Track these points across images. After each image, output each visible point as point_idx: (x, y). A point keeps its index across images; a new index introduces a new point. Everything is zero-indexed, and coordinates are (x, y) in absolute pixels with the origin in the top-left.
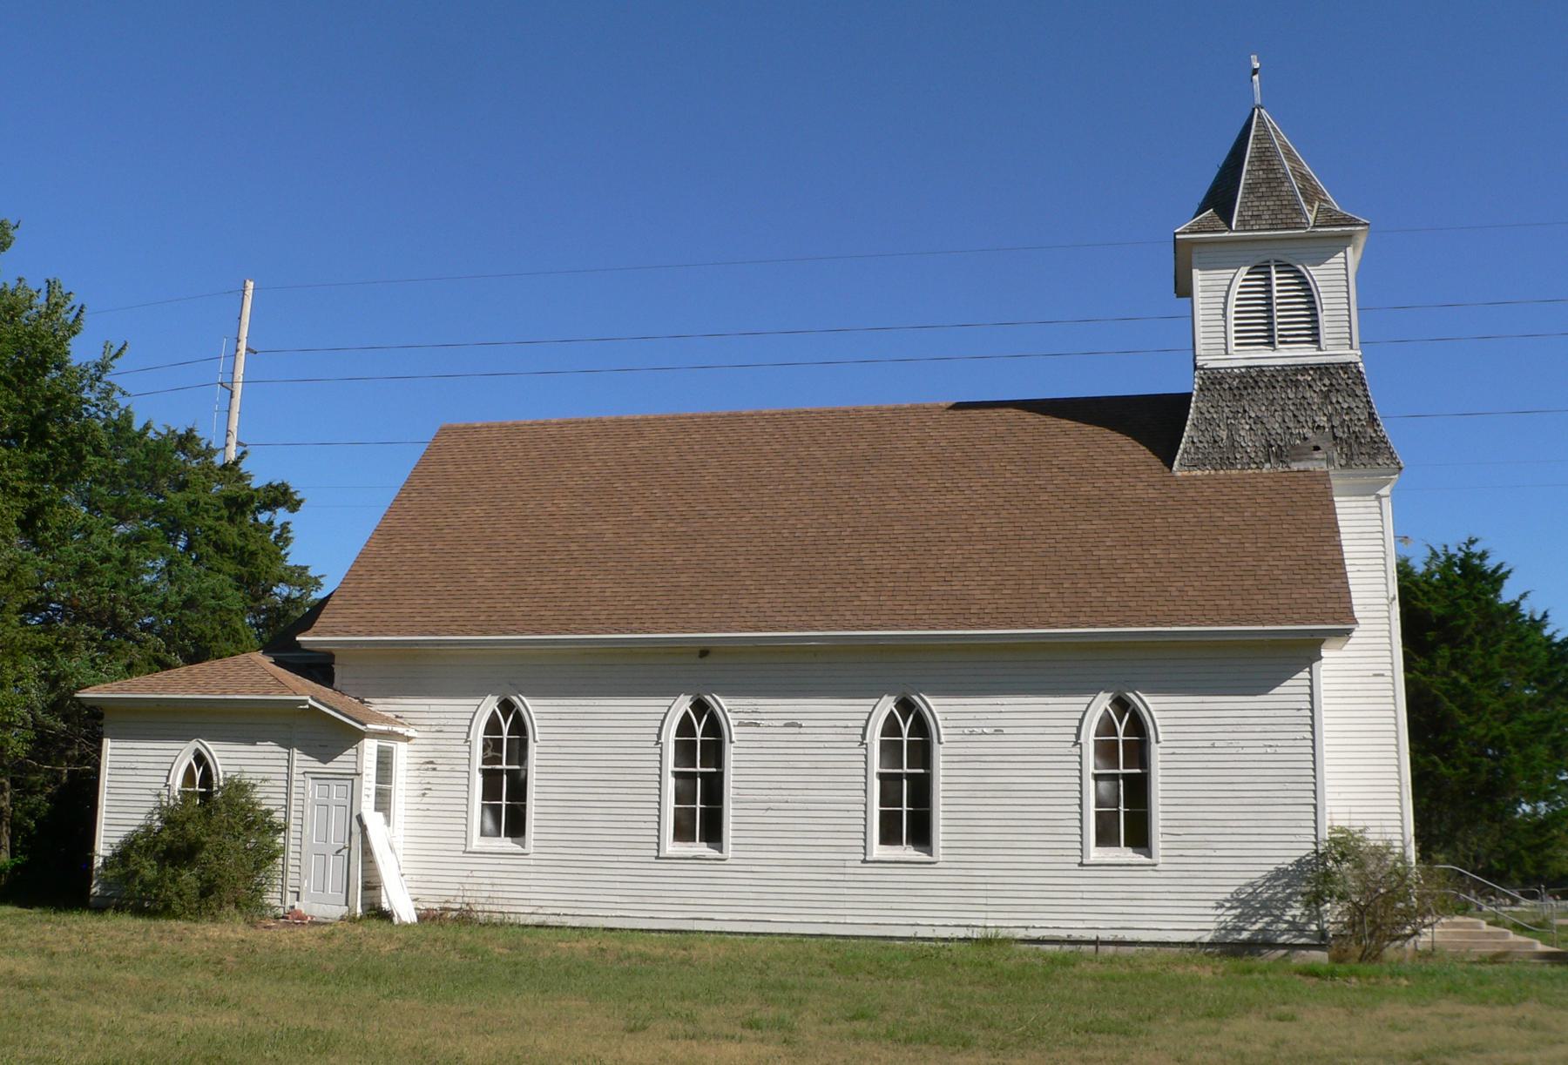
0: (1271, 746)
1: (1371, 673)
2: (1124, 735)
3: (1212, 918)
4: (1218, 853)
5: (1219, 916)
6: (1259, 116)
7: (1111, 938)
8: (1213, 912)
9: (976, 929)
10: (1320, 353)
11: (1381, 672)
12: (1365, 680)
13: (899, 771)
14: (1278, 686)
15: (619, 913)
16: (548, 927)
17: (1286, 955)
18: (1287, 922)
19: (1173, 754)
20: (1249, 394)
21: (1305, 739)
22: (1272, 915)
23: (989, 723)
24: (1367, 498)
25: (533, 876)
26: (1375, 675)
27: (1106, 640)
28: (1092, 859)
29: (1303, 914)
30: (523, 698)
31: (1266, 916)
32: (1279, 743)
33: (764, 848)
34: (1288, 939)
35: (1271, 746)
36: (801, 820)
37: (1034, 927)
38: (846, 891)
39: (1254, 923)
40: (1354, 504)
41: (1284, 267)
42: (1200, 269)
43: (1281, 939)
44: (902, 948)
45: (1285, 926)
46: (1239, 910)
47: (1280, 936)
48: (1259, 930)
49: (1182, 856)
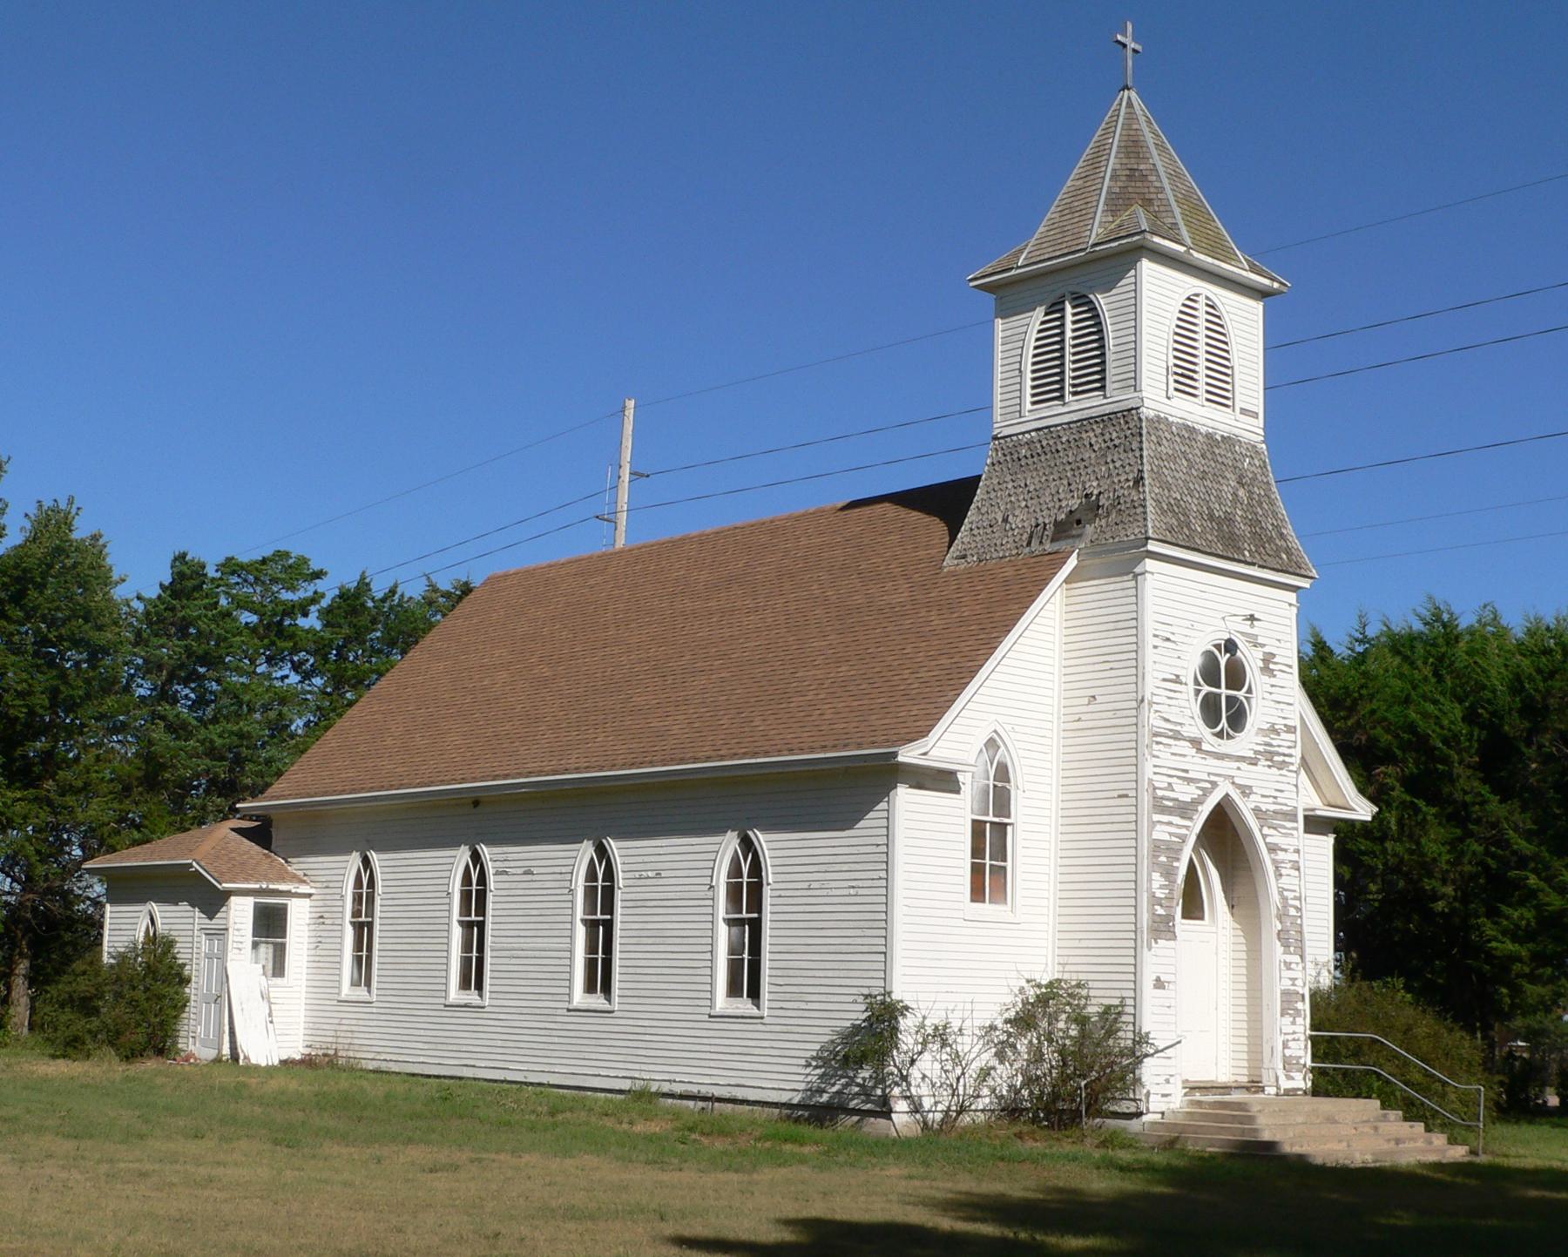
0: (853, 887)
1: (1115, 794)
2: (748, 877)
3: (801, 1078)
4: (810, 1006)
5: (808, 1075)
6: (1129, 98)
7: (728, 1096)
8: (803, 1071)
9: (637, 1081)
10: (1105, 401)
11: (1125, 792)
12: (1111, 802)
13: (594, 917)
14: (862, 819)
15: (422, 1059)
16: (382, 1072)
17: (858, 1121)
18: (858, 1085)
19: (780, 896)
20: (1034, 463)
21: (880, 878)
22: (847, 1077)
23: (648, 866)
24: (1125, 578)
25: (375, 1023)
26: (1120, 796)
27: (739, 773)
28: (575, 1004)
29: (871, 1077)
30: (758, 833)
31: (844, 1077)
32: (860, 883)
33: (508, 996)
34: (858, 1104)
35: (853, 887)
36: (531, 968)
37: (675, 1081)
38: (556, 1040)
39: (834, 1085)
40: (1112, 587)
41: (1081, 300)
42: (1002, 318)
43: (852, 1104)
44: (607, 1100)
45: (857, 1089)
46: (823, 1070)
47: (852, 1099)
48: (837, 1092)
49: (782, 1008)
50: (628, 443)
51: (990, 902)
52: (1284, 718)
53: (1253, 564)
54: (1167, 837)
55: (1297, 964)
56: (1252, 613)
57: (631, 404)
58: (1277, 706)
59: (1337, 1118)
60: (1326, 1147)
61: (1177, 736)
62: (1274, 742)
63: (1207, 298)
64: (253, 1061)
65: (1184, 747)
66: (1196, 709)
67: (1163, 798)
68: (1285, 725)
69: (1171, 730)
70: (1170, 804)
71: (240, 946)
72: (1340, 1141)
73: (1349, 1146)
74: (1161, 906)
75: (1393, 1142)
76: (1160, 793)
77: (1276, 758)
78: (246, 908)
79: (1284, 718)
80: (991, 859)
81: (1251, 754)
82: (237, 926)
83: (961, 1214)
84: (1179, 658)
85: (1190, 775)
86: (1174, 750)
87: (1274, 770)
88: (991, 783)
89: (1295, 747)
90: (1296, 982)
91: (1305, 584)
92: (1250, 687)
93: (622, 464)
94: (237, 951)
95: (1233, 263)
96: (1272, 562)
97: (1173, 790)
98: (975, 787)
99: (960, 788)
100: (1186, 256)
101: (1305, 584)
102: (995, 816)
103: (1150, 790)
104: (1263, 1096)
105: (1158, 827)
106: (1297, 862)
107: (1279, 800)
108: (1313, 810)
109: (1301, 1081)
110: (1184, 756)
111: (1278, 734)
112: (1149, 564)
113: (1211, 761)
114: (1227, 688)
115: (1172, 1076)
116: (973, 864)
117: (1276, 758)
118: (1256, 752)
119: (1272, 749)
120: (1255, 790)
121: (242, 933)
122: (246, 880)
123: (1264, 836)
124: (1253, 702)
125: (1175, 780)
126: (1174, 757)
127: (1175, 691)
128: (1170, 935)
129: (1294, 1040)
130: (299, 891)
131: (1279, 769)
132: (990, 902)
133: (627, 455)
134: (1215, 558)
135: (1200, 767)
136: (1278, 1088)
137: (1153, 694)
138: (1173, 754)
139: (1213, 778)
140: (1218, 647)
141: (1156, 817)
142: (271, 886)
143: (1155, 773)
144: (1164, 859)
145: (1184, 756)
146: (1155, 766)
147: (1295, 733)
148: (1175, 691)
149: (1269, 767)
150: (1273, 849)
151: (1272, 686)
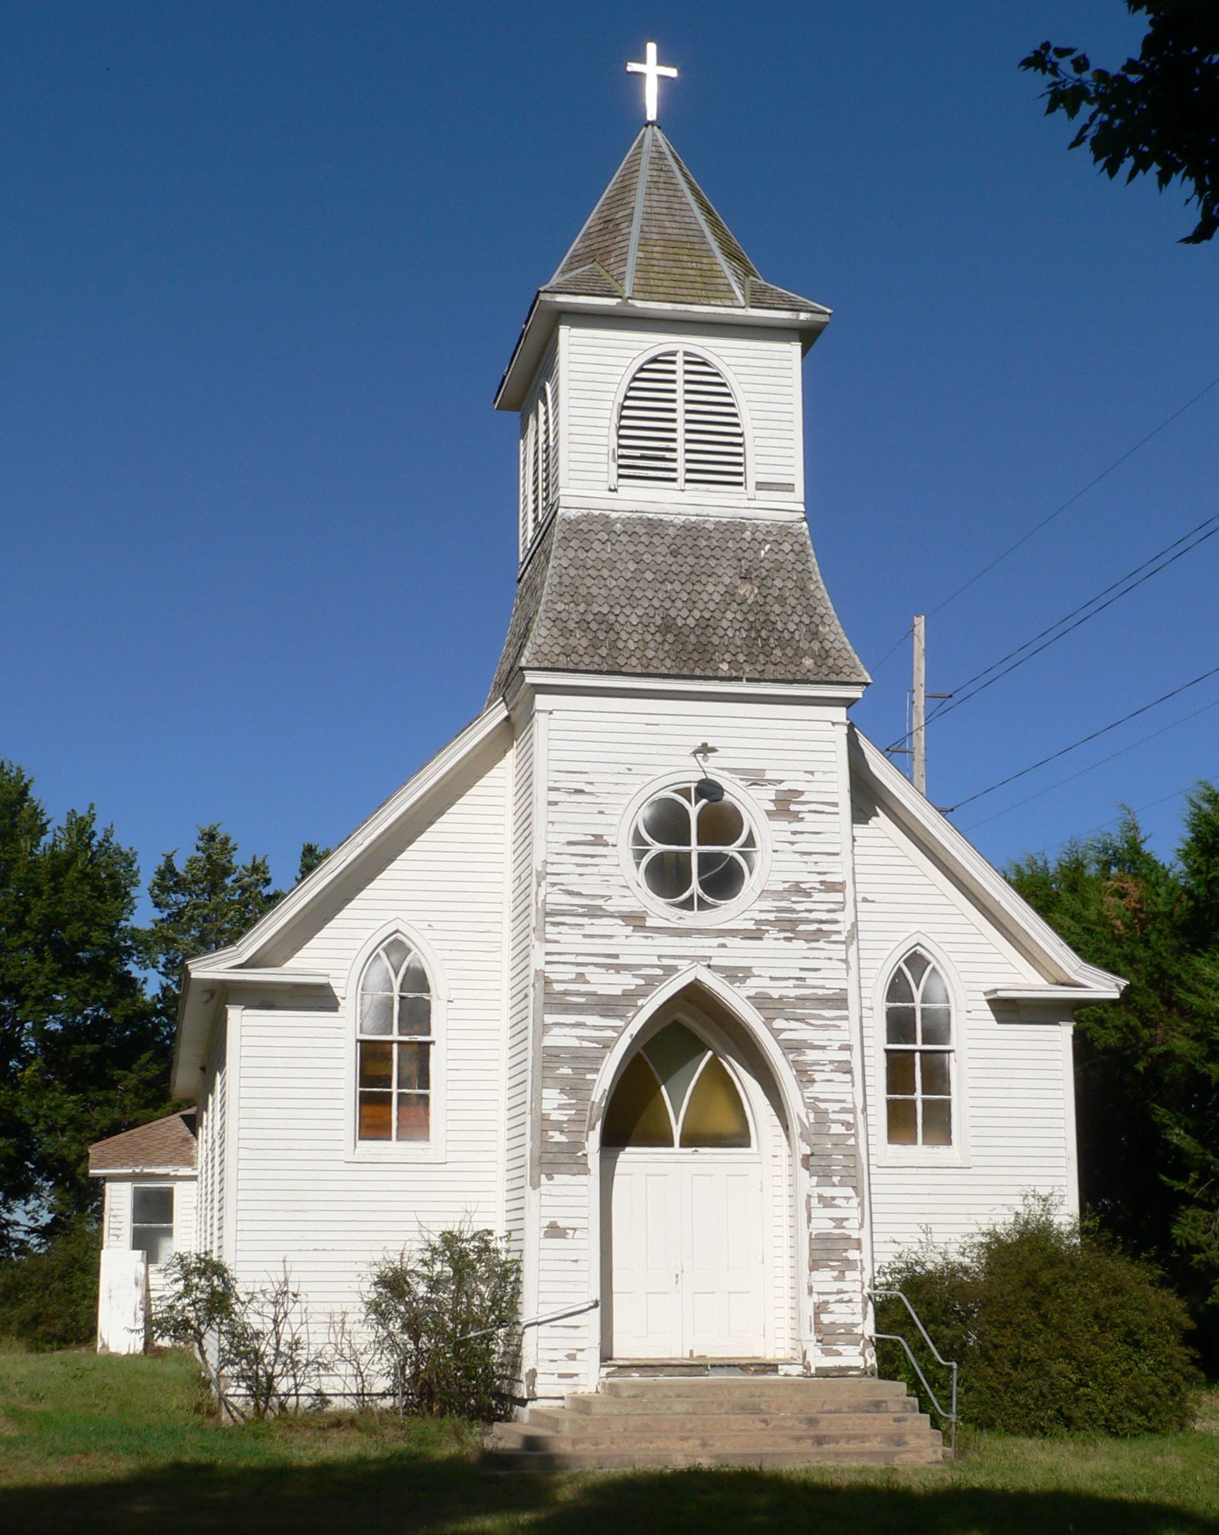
50: (920, 665)
52: (819, 873)
53: (738, 679)
55: (848, 1198)
56: (704, 740)
57: (920, 623)
61: (595, 912)
62: (798, 907)
63: (686, 354)
64: (112, 1350)
66: (640, 876)
67: (565, 993)
68: (822, 883)
70: (582, 1000)
71: (117, 1232)
74: (562, 1132)
76: (558, 987)
77: (802, 928)
78: (123, 1194)
79: (819, 873)
80: (399, 1087)
81: (751, 925)
82: (113, 1213)
84: (600, 812)
85: (622, 960)
86: (588, 931)
87: (801, 944)
88: (396, 994)
89: (843, 910)
91: (856, 693)
93: (915, 688)
94: (115, 1238)
96: (780, 672)
97: (588, 983)
98: (368, 999)
99: (338, 1004)
100: (625, 308)
101: (856, 693)
102: (401, 1033)
103: (541, 983)
104: (777, 1377)
105: (556, 1031)
106: (849, 1062)
107: (808, 982)
108: (996, 991)
109: (857, 1357)
110: (611, 937)
111: (809, 895)
112: (541, 701)
114: (700, 843)
116: (889, 1102)
117: (802, 928)
118: (758, 922)
119: (795, 916)
120: (755, 971)
121: (119, 1219)
122: (122, 1166)
123: (775, 1033)
124: (757, 859)
125: (591, 968)
127: (593, 856)
129: (837, 1302)
130: (179, 1173)
132: (924, 1143)
133: (920, 677)
134: (662, 680)
136: (808, 1367)
137: (546, 862)
138: (585, 936)
139: (666, 962)
141: (549, 1019)
142: (146, 1170)
143: (548, 963)
146: (547, 954)
147: (842, 891)
148: (593, 856)
149: (786, 939)
150: (791, 1047)
151: (794, 833)
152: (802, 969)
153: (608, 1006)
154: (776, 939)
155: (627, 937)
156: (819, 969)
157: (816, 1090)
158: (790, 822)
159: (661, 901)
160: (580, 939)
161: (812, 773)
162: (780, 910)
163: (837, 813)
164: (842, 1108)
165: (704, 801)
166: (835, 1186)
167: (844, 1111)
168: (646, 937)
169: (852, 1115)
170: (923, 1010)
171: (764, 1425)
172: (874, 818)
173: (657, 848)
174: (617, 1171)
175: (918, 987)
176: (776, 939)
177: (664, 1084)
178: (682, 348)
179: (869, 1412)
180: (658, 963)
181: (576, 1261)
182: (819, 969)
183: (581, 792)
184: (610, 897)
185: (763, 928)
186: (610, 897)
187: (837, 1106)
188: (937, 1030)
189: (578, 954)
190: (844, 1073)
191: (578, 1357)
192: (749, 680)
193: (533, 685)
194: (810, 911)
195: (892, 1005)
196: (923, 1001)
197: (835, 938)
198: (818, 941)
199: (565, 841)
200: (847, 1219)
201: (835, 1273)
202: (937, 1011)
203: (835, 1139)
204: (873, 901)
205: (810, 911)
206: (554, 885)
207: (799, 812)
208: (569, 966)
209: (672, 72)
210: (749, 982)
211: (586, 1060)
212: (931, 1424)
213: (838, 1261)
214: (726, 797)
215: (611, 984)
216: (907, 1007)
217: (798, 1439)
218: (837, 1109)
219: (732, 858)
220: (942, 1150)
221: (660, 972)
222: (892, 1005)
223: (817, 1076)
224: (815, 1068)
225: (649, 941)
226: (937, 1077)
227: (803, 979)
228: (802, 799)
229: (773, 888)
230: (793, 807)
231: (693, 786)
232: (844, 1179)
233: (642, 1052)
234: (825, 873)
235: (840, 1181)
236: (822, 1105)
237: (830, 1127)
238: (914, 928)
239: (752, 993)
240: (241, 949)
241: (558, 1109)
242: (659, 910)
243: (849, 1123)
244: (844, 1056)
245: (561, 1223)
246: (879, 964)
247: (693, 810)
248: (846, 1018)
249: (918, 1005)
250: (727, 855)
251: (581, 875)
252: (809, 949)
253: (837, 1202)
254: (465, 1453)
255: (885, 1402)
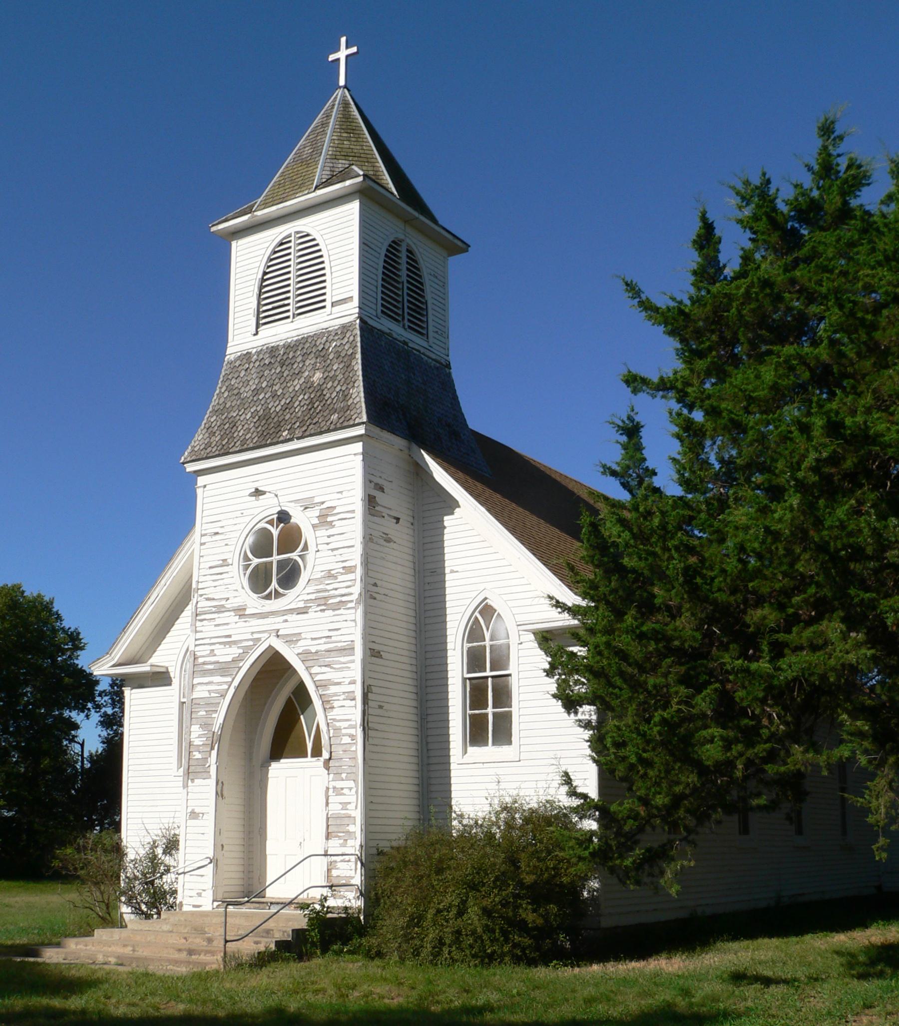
51: (493, 744)
52: (343, 561)
54: (207, 695)
55: (350, 789)
58: (335, 552)
59: (206, 929)
60: (110, 949)
61: (220, 610)
63: (298, 232)
65: (230, 617)
67: (204, 663)
68: (344, 568)
69: (214, 607)
72: (125, 946)
73: (134, 951)
75: (185, 953)
77: (331, 601)
79: (343, 561)
81: (301, 605)
83: (488, 1016)
85: (233, 638)
86: (218, 622)
87: (330, 613)
90: (349, 807)
92: (306, 544)
95: (289, 198)
105: (199, 688)
107: (333, 639)
110: (227, 624)
111: (336, 578)
112: (201, 480)
113: (254, 622)
115: (204, 890)
117: (331, 601)
118: (306, 601)
126: (217, 628)
127: (221, 574)
128: (205, 775)
129: (342, 861)
131: (334, 610)
132: (493, 744)
135: (241, 630)
138: (216, 625)
139: (256, 636)
140: (271, 522)
144: (203, 713)
145: (227, 624)
148: (221, 574)
149: (322, 610)
151: (329, 537)
152: (330, 630)
153: (224, 669)
154: (316, 612)
155: (236, 623)
156: (340, 629)
157: (332, 714)
158: (327, 530)
159: (255, 596)
160: (213, 628)
161: (341, 492)
162: (319, 591)
163: (354, 518)
164: (349, 725)
165: (282, 525)
166: (343, 780)
167: (350, 727)
168: (246, 621)
169: (354, 730)
170: (491, 646)
171: (185, 941)
172: (457, 510)
173: (256, 561)
174: (270, 775)
175: (488, 629)
176: (316, 612)
177: (302, 714)
178: (292, 231)
179: (263, 937)
180: (251, 637)
181: (203, 834)
182: (340, 629)
183: (217, 533)
184: (228, 599)
185: (308, 605)
186: (228, 599)
187: (346, 724)
188: (500, 660)
189: (211, 638)
190: (351, 700)
191: (203, 895)
192: (298, 438)
193: (195, 472)
194: (336, 589)
195: (471, 645)
196: (491, 640)
197: (350, 605)
198: (340, 609)
199: (207, 567)
200: (350, 803)
201: (342, 841)
202: (500, 646)
203: (344, 747)
204: (457, 572)
205: (336, 589)
206: (201, 595)
207: (333, 521)
208: (206, 646)
209: (343, 40)
210: (300, 643)
211: (211, 705)
212: (90, 936)
213: (343, 832)
214: (292, 520)
215: (226, 654)
216: (481, 646)
217: (180, 950)
218: (346, 726)
219: (295, 560)
220: (505, 748)
221: (251, 643)
222: (471, 645)
223: (336, 704)
224: (334, 698)
225: (247, 624)
226: (503, 695)
227: (330, 637)
228: (335, 512)
229: (315, 577)
230: (329, 519)
231: (275, 516)
232: (349, 775)
233: (292, 696)
234: (346, 561)
235: (346, 777)
236: (338, 724)
237: (341, 739)
238: (481, 587)
239: (300, 651)
240: (113, 655)
241: (198, 737)
242: (253, 602)
243: (353, 736)
244: (351, 688)
245: (197, 810)
246: (459, 616)
247: (275, 532)
248: (353, 661)
249: (487, 643)
250: (292, 559)
251: (215, 587)
252: (334, 616)
253: (345, 791)
254: (763, 986)
255: (273, 930)
